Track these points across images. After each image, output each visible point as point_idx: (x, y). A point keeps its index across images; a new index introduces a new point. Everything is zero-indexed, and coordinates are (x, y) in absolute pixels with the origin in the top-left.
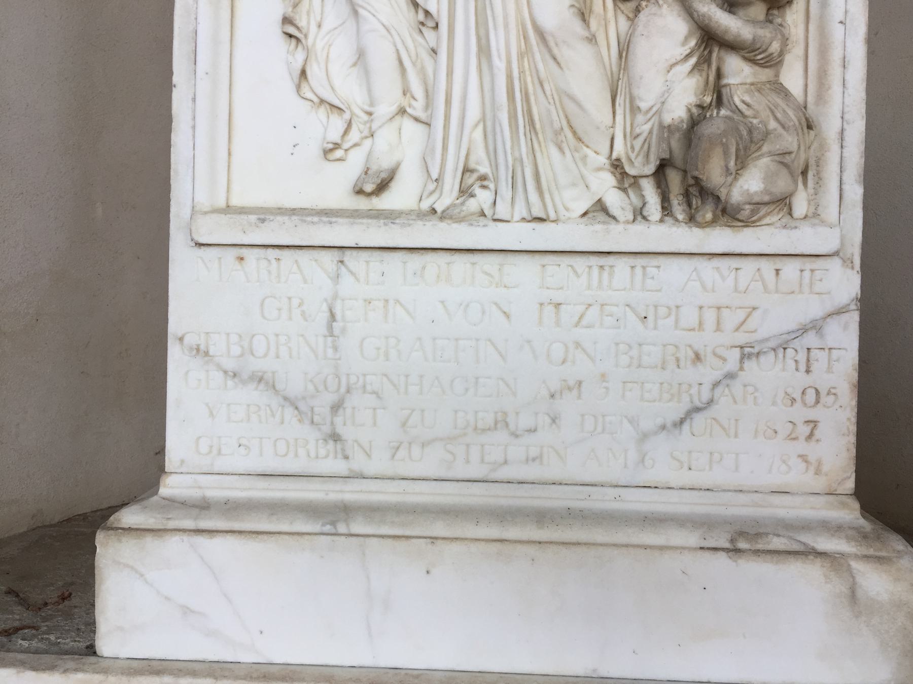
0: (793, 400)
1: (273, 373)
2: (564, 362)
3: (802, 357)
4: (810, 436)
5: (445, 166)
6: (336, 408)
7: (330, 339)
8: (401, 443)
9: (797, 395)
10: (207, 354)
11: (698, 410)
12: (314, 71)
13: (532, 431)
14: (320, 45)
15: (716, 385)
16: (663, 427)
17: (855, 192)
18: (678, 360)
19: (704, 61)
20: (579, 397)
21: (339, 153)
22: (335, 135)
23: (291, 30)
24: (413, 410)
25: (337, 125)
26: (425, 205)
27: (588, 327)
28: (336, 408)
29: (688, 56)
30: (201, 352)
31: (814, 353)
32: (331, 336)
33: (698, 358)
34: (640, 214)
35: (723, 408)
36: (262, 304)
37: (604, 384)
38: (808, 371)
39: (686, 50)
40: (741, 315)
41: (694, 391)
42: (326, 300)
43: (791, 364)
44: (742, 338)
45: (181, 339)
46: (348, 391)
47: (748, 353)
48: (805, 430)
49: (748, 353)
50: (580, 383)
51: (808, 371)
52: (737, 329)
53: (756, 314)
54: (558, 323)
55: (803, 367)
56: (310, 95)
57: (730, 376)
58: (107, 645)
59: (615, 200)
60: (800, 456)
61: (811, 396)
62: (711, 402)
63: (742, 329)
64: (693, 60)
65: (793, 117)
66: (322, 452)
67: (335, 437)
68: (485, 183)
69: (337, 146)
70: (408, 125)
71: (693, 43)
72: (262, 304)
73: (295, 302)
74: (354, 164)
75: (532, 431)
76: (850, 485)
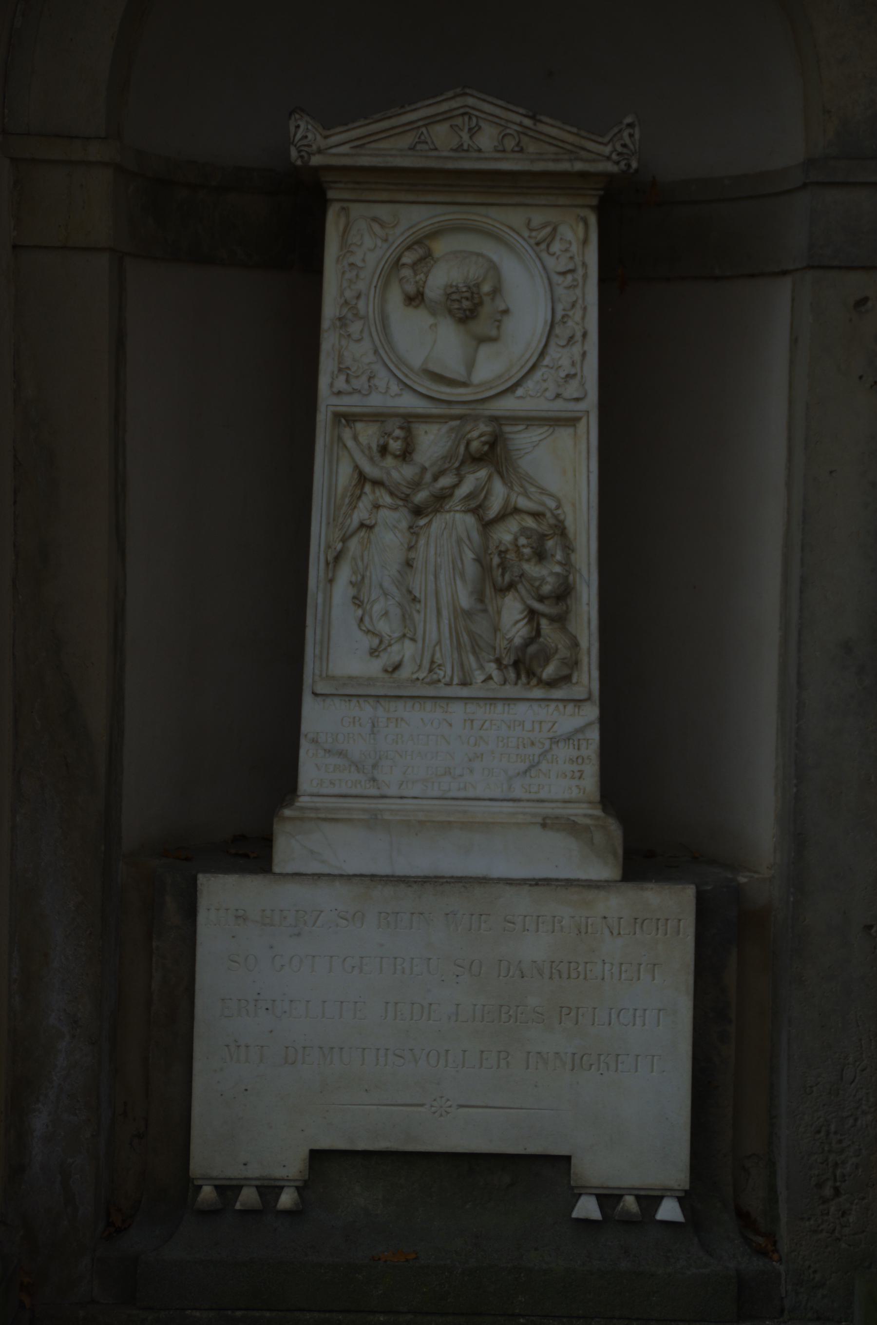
0: (573, 761)
1: (347, 750)
2: (475, 745)
3: (576, 743)
4: (580, 778)
5: (426, 422)
6: (375, 766)
7: (372, 735)
8: (403, 781)
9: (575, 759)
10: (317, 742)
11: (533, 766)
12: (367, 619)
13: (461, 776)
14: (368, 607)
15: (540, 755)
16: (518, 774)
17: (595, 674)
18: (524, 744)
19: (530, 621)
20: (482, 761)
21: (376, 654)
22: (375, 645)
23: (357, 602)
24: (486, 721)
25: (376, 641)
26: (415, 676)
27: (487, 730)
28: (375, 766)
29: (523, 619)
30: (315, 741)
31: (581, 742)
32: (373, 734)
33: (533, 744)
34: (505, 682)
35: (544, 766)
36: (342, 720)
37: (493, 755)
38: (579, 749)
39: (522, 616)
40: (550, 725)
41: (531, 758)
42: (371, 718)
43: (571, 746)
44: (551, 735)
45: (306, 736)
46: (380, 758)
47: (555, 741)
48: (577, 774)
49: (555, 741)
50: (482, 755)
51: (579, 749)
52: (549, 731)
53: (556, 725)
54: (472, 728)
55: (576, 747)
56: (364, 628)
57: (547, 751)
58: (276, 869)
59: (495, 674)
60: (577, 786)
61: (580, 761)
62: (538, 763)
63: (551, 731)
64: (525, 621)
65: (568, 642)
66: (368, 786)
67: (374, 780)
68: (441, 668)
69: (376, 650)
70: (407, 643)
71: (525, 613)
72: (342, 720)
73: (357, 719)
74: (385, 660)
75: (461, 776)
76: (596, 797)
